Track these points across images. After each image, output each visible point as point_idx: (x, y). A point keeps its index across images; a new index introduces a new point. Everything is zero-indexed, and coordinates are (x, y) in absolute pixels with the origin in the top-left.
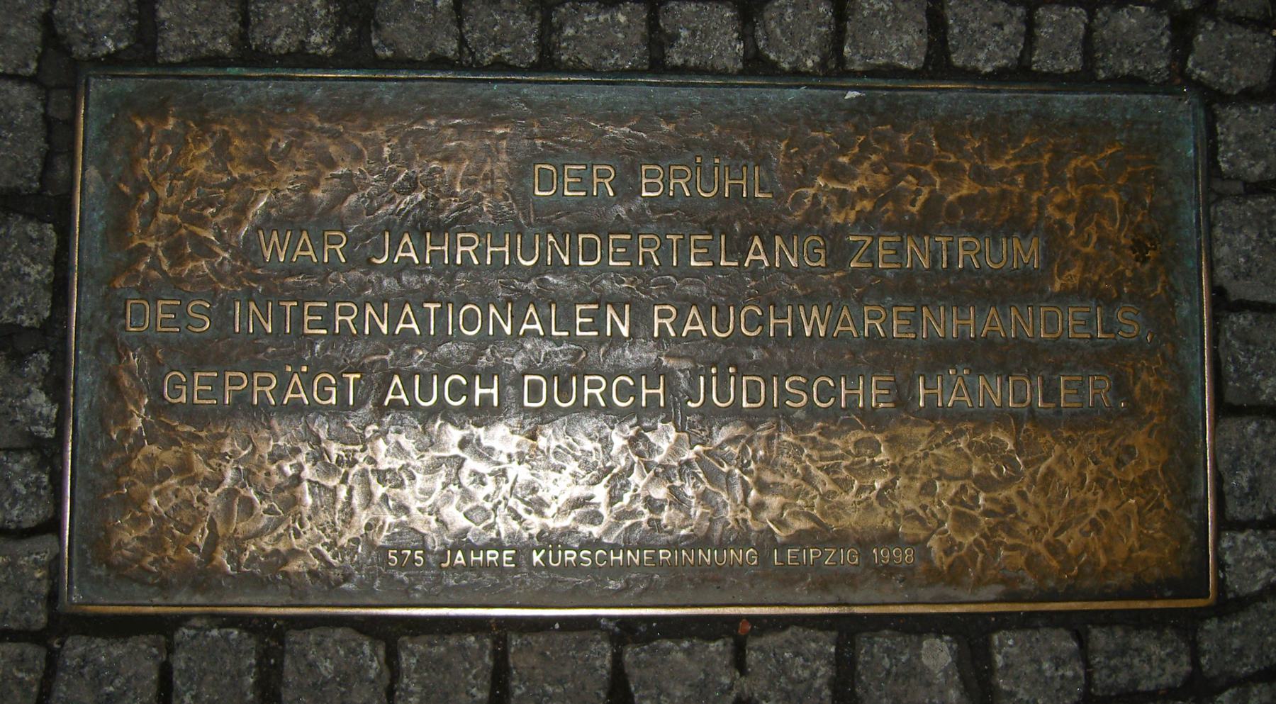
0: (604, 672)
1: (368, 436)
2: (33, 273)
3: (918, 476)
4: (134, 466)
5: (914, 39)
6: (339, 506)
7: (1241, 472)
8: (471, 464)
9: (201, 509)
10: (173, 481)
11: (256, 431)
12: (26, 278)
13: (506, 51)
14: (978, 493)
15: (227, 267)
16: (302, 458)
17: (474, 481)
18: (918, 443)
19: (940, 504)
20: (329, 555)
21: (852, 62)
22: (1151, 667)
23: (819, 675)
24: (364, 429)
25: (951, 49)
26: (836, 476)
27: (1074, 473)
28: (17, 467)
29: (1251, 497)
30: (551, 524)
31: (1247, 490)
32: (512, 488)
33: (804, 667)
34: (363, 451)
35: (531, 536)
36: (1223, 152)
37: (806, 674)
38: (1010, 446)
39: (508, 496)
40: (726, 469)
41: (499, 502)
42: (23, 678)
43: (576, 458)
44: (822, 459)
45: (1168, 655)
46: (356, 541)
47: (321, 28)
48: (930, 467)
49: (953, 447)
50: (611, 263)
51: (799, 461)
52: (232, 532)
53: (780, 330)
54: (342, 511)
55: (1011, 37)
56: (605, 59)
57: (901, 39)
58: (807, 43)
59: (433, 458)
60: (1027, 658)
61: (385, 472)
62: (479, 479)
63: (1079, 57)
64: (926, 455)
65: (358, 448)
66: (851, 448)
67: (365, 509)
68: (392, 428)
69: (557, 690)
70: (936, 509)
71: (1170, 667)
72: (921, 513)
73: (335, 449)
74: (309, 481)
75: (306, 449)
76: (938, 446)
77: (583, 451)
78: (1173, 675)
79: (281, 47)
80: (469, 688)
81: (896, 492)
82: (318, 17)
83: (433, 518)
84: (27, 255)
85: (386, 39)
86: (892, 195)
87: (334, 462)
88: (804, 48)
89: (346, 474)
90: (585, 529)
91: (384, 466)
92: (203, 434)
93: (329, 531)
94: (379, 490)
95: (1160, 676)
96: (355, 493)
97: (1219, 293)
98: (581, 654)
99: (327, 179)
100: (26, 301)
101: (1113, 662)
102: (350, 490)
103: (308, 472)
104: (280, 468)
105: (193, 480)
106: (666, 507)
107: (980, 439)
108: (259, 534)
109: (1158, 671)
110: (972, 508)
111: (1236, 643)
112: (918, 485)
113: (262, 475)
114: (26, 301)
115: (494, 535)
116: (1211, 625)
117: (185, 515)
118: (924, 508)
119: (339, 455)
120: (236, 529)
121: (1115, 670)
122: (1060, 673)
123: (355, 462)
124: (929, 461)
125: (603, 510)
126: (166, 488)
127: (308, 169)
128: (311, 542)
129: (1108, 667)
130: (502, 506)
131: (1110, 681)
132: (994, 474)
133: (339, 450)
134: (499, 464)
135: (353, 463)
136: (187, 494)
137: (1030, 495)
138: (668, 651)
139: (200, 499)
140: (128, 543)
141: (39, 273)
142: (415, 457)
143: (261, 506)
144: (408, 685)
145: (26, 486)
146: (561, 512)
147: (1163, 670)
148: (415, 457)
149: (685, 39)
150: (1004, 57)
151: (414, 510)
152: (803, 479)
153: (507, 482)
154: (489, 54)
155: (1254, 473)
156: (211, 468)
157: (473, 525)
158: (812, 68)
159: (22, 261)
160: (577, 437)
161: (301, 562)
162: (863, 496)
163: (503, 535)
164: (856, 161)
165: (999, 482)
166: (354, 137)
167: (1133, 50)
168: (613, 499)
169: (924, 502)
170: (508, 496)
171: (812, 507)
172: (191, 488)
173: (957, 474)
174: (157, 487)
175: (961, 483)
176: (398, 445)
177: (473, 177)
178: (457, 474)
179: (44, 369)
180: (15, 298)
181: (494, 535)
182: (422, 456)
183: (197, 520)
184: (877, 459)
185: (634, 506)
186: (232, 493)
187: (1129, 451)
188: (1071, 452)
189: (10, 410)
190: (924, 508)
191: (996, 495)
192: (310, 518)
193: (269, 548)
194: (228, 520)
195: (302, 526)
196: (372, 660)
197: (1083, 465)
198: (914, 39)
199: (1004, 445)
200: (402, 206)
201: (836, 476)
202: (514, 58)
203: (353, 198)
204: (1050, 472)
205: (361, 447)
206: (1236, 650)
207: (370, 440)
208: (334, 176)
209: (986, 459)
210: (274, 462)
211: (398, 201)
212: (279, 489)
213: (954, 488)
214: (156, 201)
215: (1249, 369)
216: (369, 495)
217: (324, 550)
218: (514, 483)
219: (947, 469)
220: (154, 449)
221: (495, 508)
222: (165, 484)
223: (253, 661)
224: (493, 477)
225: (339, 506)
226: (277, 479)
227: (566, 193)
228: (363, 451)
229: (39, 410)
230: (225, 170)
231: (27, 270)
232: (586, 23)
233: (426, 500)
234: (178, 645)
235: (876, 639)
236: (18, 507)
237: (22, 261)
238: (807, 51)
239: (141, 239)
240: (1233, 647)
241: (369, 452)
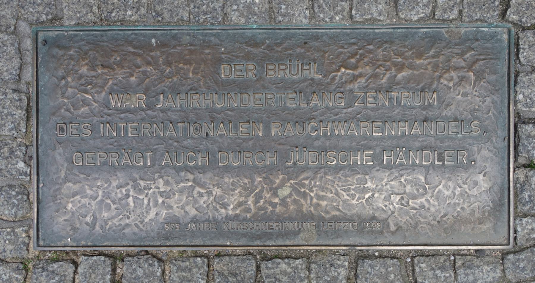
0: (253, 272)
1: (156, 178)
2: (17, 114)
3: (383, 193)
4: (62, 191)
5: (383, 6)
6: (144, 206)
7: (525, 192)
8: (198, 189)
9: (90, 208)
10: (78, 197)
11: (111, 176)
12: (14, 116)
13: (209, 16)
14: (408, 200)
15: (97, 109)
16: (129, 187)
17: (199, 196)
18: (383, 179)
19: (393, 205)
20: (141, 226)
21: (356, 18)
22: (483, 274)
23: (341, 274)
24: (154, 175)
25: (399, 10)
26: (348, 193)
27: (450, 192)
28: (14, 193)
29: (529, 203)
30: (230, 213)
31: (528, 200)
32: (215, 198)
33: (335, 271)
34: (154, 184)
35: (222, 218)
36: (522, 53)
37: (336, 274)
38: (423, 180)
39: (213, 202)
40: (303, 190)
41: (209, 204)
42: (17, 277)
43: (241, 186)
44: (343, 186)
45: (491, 269)
46: (151, 220)
47: (131, 8)
48: (388, 189)
49: (398, 181)
50: (220, 164)
51: (334, 187)
52: (102, 217)
53: (325, 133)
54: (146, 208)
55: (426, 4)
56: (250, 19)
57: (377, 7)
58: (336, 9)
59: (182, 186)
60: (429, 268)
61: (163, 192)
62: (201, 195)
63: (457, 12)
64: (386, 184)
65: (152, 182)
66: (355, 181)
67: (155, 207)
68: (166, 174)
69: (234, 280)
70: (391, 207)
71: (492, 275)
72: (384, 208)
73: (142, 183)
74: (133, 196)
75: (131, 183)
76: (392, 181)
77: (243, 183)
78: (493, 278)
79: (115, 17)
80: (198, 279)
81: (374, 199)
82: (129, 4)
83: (182, 211)
84: (14, 106)
85: (158, 13)
86: (375, 76)
87: (142, 189)
88: (335, 11)
89: (147, 193)
90: (243, 215)
91: (162, 190)
92: (89, 178)
93: (141, 216)
94: (160, 200)
95: (487, 278)
96: (151, 200)
97: (518, 115)
98: (243, 265)
99: (137, 73)
100: (15, 125)
101: (466, 272)
102: (149, 200)
103: (131, 193)
104: (121, 191)
105: (86, 197)
106: (278, 206)
107: (410, 178)
108: (113, 218)
109: (487, 276)
110: (406, 206)
111: (522, 265)
112: (383, 196)
113: (113, 194)
114: (15, 125)
115: (207, 217)
116: (511, 257)
117: (83, 211)
118: (386, 206)
119: (144, 185)
120: (104, 216)
121: (467, 275)
122: (443, 275)
123: (151, 188)
124: (388, 186)
125: (252, 207)
126: (75, 200)
127: (129, 69)
128: (133, 221)
129: (465, 274)
130: (211, 205)
131: (465, 280)
132: (416, 192)
133: (145, 183)
134: (209, 188)
135: (150, 189)
136: (84, 202)
137: (431, 201)
138: (279, 263)
139: (89, 204)
140: (61, 222)
141: (20, 114)
142: (175, 186)
143: (113, 207)
144: (173, 278)
145: (18, 200)
146: (234, 209)
147: (489, 275)
148: (175, 186)
149: (283, 9)
150: (423, 13)
151: (175, 206)
152: (335, 194)
153: (212, 196)
154: (201, 18)
155: (531, 193)
156: (94, 191)
157: (199, 214)
158: (339, 20)
159: (12, 109)
160: (241, 178)
161: (130, 229)
162: (360, 201)
163: (211, 218)
164: (358, 61)
165: (418, 196)
166: (147, 55)
167: (482, 8)
168: (256, 202)
169: (385, 204)
170: (213, 202)
171: (339, 205)
172: (85, 200)
173: (400, 193)
174: (72, 199)
175: (400, 196)
176: (168, 181)
177: (197, 71)
178: (192, 193)
179: (23, 153)
180: (10, 124)
181: (207, 217)
182: (178, 186)
183: (88, 213)
184: (366, 186)
185: (265, 205)
186: (102, 201)
187: (476, 183)
188: (450, 184)
189: (10, 170)
190: (386, 206)
191: (416, 201)
192: (133, 211)
193: (117, 224)
194: (100, 213)
195: (130, 214)
196: (158, 269)
197: (455, 188)
198: (383, 6)
199: (420, 180)
200: (168, 83)
201: (348, 193)
202: (212, 19)
203: (147, 80)
204: (440, 191)
205: (153, 182)
206: (521, 267)
207: (157, 179)
208: (139, 72)
209: (412, 186)
210: (118, 189)
211: (166, 81)
212: (121, 199)
213: (398, 197)
214: (67, 82)
215: (530, 148)
216: (156, 202)
217: (139, 224)
218: (215, 196)
219: (396, 190)
220: (70, 184)
221: (208, 206)
222: (75, 198)
223: (110, 269)
224: (207, 194)
225: (144, 206)
226: (119, 195)
227: (374, 134)
228: (154, 184)
229: (22, 169)
230: (94, 70)
231: (15, 113)
232: (241, 3)
233: (180, 203)
234: (81, 263)
235: (365, 260)
236: (15, 209)
237: (12, 109)
238: (336, 13)
239: (62, 99)
240: (520, 266)
241: (156, 184)
